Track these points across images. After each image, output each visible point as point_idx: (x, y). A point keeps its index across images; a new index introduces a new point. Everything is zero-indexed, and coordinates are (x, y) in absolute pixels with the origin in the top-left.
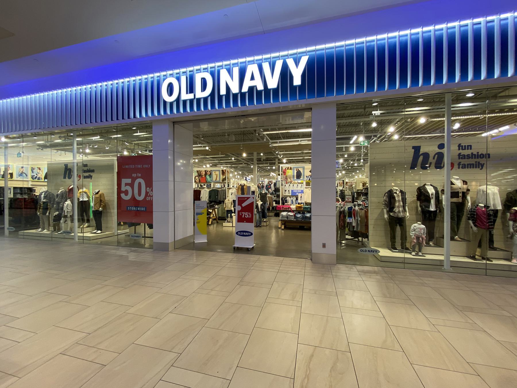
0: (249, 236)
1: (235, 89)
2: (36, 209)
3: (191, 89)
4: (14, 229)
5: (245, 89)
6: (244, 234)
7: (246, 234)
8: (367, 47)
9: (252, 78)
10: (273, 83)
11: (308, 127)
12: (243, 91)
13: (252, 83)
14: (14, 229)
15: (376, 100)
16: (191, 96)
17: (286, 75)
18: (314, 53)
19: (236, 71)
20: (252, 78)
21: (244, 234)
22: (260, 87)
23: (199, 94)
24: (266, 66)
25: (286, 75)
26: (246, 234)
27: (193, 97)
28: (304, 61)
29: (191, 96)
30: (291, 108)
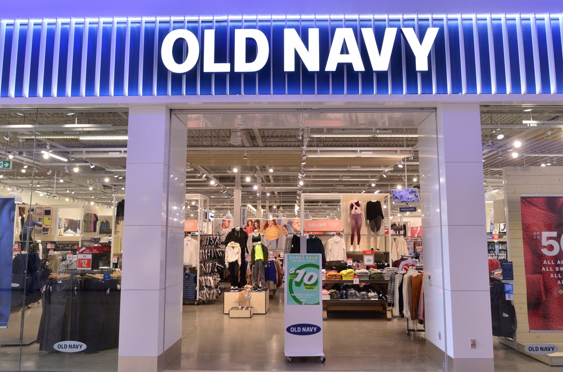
0: (313, 333)
1: (313, 65)
2: (494, 242)
3: (224, 52)
4: (84, 347)
5: (331, 67)
6: (304, 329)
7: (308, 329)
8: (132, 29)
9: (344, 50)
10: (381, 62)
11: (64, 156)
12: (327, 69)
13: (345, 59)
14: (84, 347)
15: (530, 105)
16: (225, 67)
17: (402, 54)
18: (269, 24)
19: (314, 35)
20: (344, 50)
21: (304, 329)
22: (359, 66)
23: (241, 65)
24: (369, 35)
25: (402, 54)
26: (308, 329)
27: (228, 70)
28: (431, 34)
29: (225, 67)
30: (387, 105)
